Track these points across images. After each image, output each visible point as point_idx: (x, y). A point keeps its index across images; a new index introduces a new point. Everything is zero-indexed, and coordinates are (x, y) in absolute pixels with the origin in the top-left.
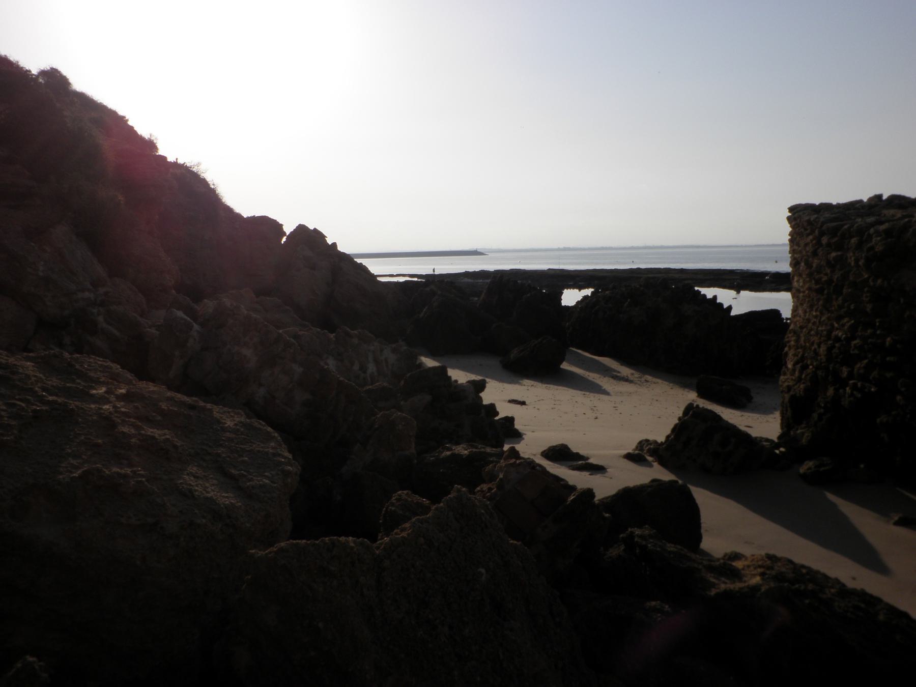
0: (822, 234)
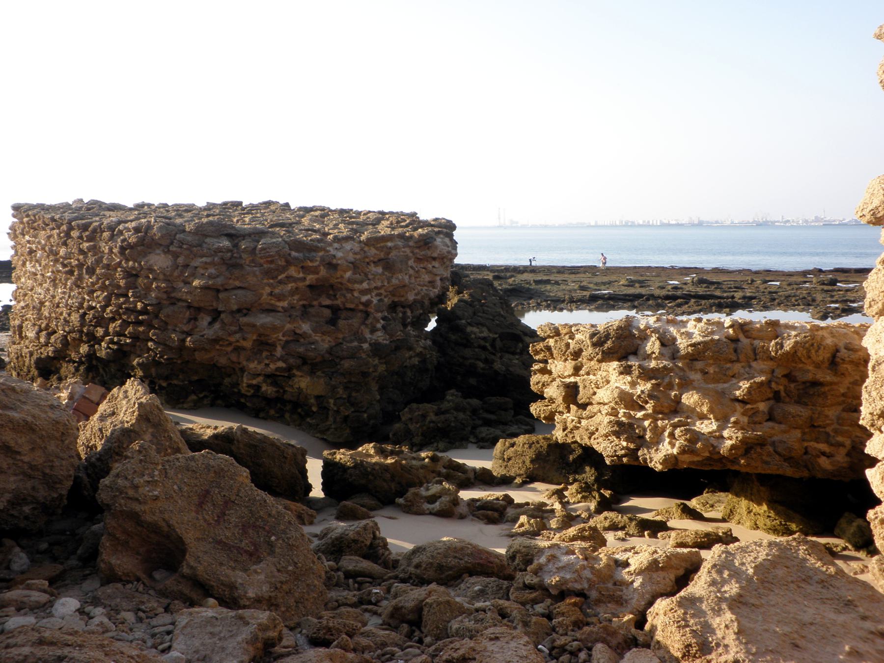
0: (71, 228)
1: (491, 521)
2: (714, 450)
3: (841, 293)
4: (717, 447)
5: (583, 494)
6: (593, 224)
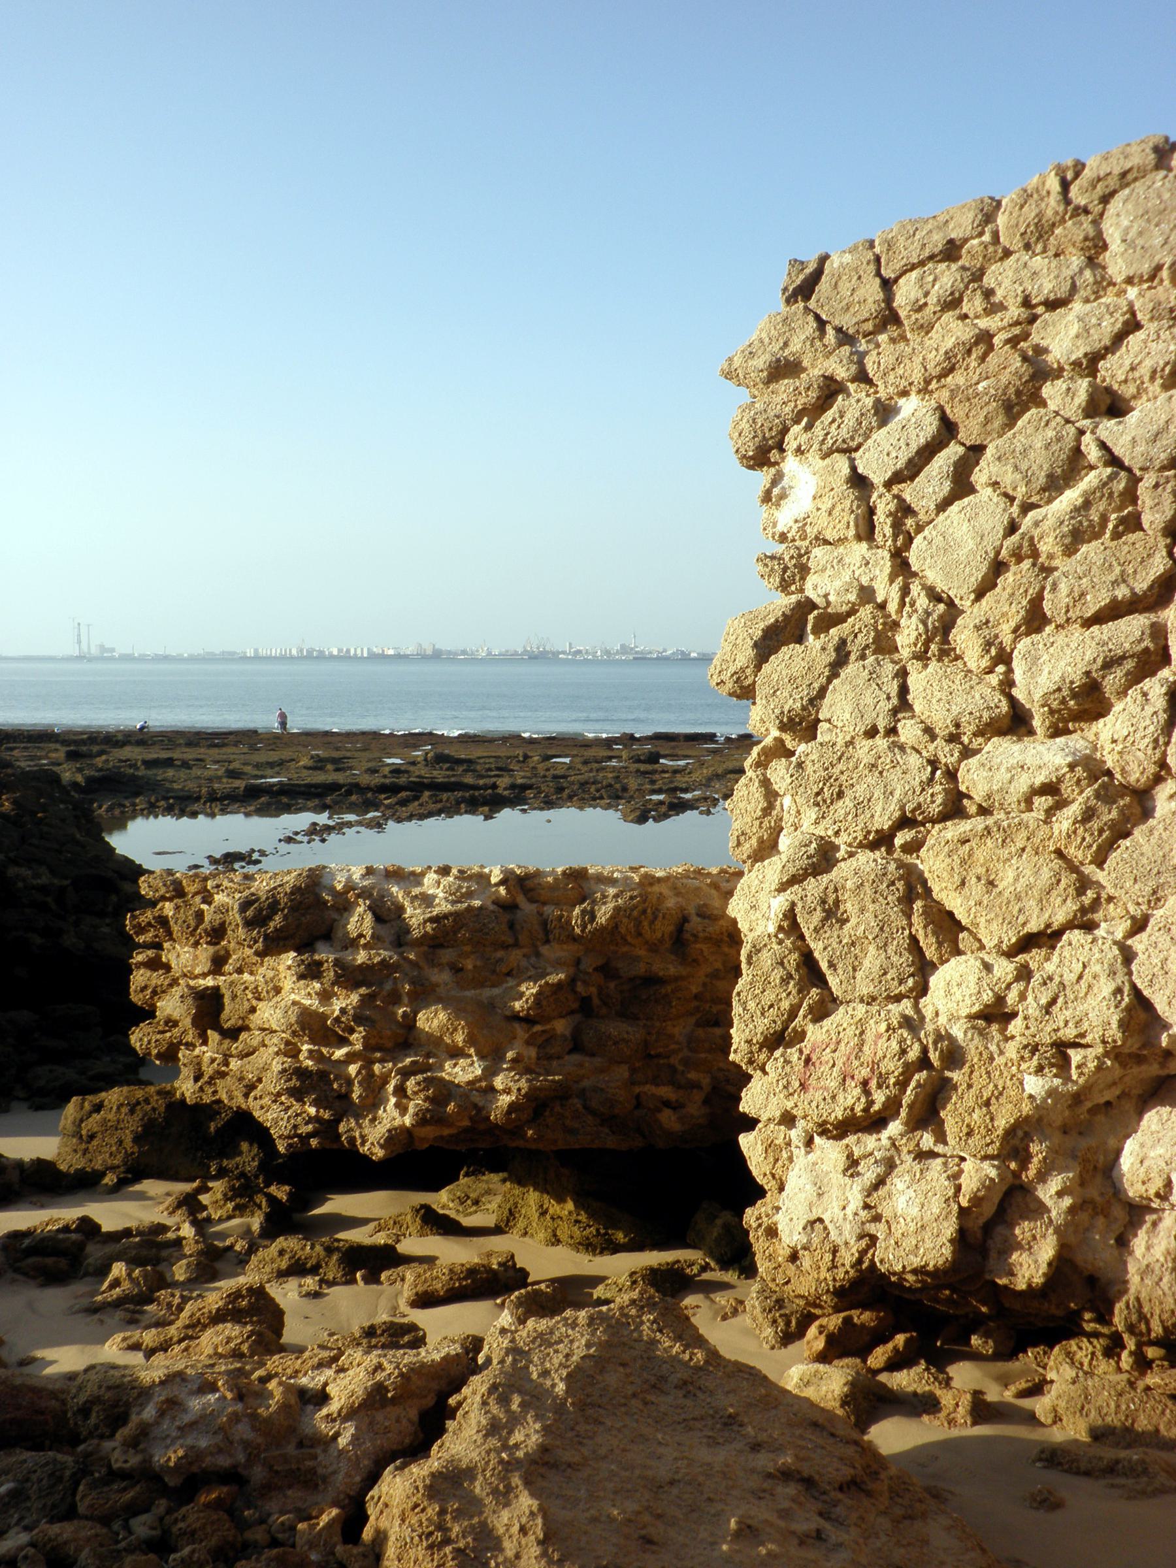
1: (53, 1278)
2: (479, 1114)
3: (666, 775)
4: (483, 1108)
5: (238, 1200)
6: (250, 653)
